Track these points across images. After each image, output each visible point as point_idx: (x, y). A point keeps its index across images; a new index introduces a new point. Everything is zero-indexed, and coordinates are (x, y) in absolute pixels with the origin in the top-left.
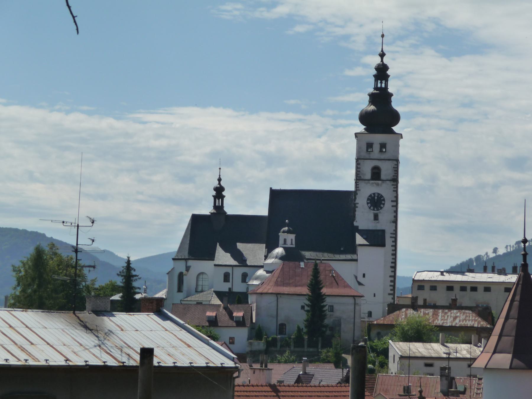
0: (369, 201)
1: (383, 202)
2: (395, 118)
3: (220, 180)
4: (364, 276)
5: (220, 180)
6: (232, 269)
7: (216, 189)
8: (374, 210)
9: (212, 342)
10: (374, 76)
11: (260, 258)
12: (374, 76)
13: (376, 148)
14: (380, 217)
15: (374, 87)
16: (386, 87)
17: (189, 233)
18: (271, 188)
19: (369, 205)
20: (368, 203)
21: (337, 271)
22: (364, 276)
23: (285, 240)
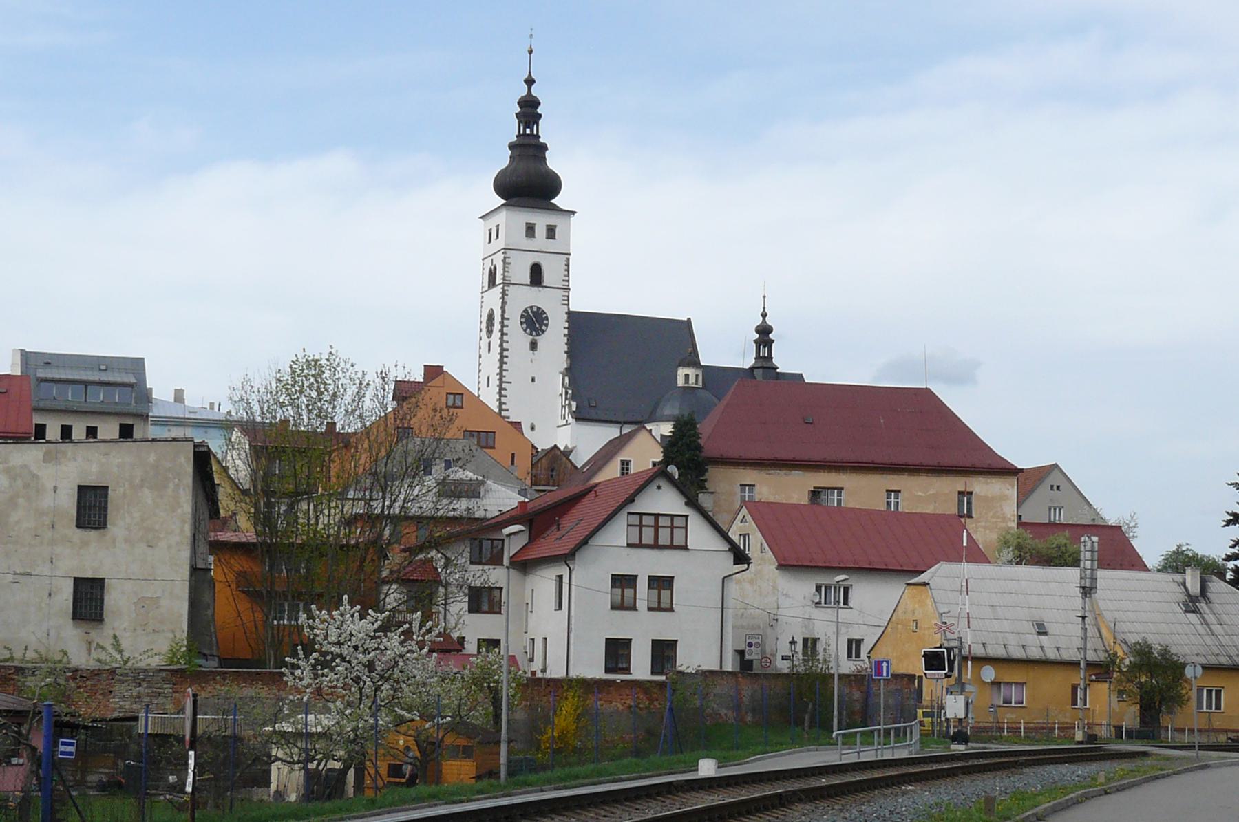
0: (523, 320)
1: (545, 322)
2: (772, 358)
3: (764, 315)
4: (533, 428)
5: (764, 315)
6: (678, 529)
7: (762, 315)
8: (531, 334)
9: (748, 759)
10: (756, 341)
11: (240, 698)
12: (756, 341)
13: (541, 231)
14: (539, 345)
15: (517, 133)
16: (770, 358)
17: (1007, 467)
18: (555, 226)
19: (524, 326)
20: (522, 323)
21: (186, 554)
22: (533, 428)
23: (687, 376)
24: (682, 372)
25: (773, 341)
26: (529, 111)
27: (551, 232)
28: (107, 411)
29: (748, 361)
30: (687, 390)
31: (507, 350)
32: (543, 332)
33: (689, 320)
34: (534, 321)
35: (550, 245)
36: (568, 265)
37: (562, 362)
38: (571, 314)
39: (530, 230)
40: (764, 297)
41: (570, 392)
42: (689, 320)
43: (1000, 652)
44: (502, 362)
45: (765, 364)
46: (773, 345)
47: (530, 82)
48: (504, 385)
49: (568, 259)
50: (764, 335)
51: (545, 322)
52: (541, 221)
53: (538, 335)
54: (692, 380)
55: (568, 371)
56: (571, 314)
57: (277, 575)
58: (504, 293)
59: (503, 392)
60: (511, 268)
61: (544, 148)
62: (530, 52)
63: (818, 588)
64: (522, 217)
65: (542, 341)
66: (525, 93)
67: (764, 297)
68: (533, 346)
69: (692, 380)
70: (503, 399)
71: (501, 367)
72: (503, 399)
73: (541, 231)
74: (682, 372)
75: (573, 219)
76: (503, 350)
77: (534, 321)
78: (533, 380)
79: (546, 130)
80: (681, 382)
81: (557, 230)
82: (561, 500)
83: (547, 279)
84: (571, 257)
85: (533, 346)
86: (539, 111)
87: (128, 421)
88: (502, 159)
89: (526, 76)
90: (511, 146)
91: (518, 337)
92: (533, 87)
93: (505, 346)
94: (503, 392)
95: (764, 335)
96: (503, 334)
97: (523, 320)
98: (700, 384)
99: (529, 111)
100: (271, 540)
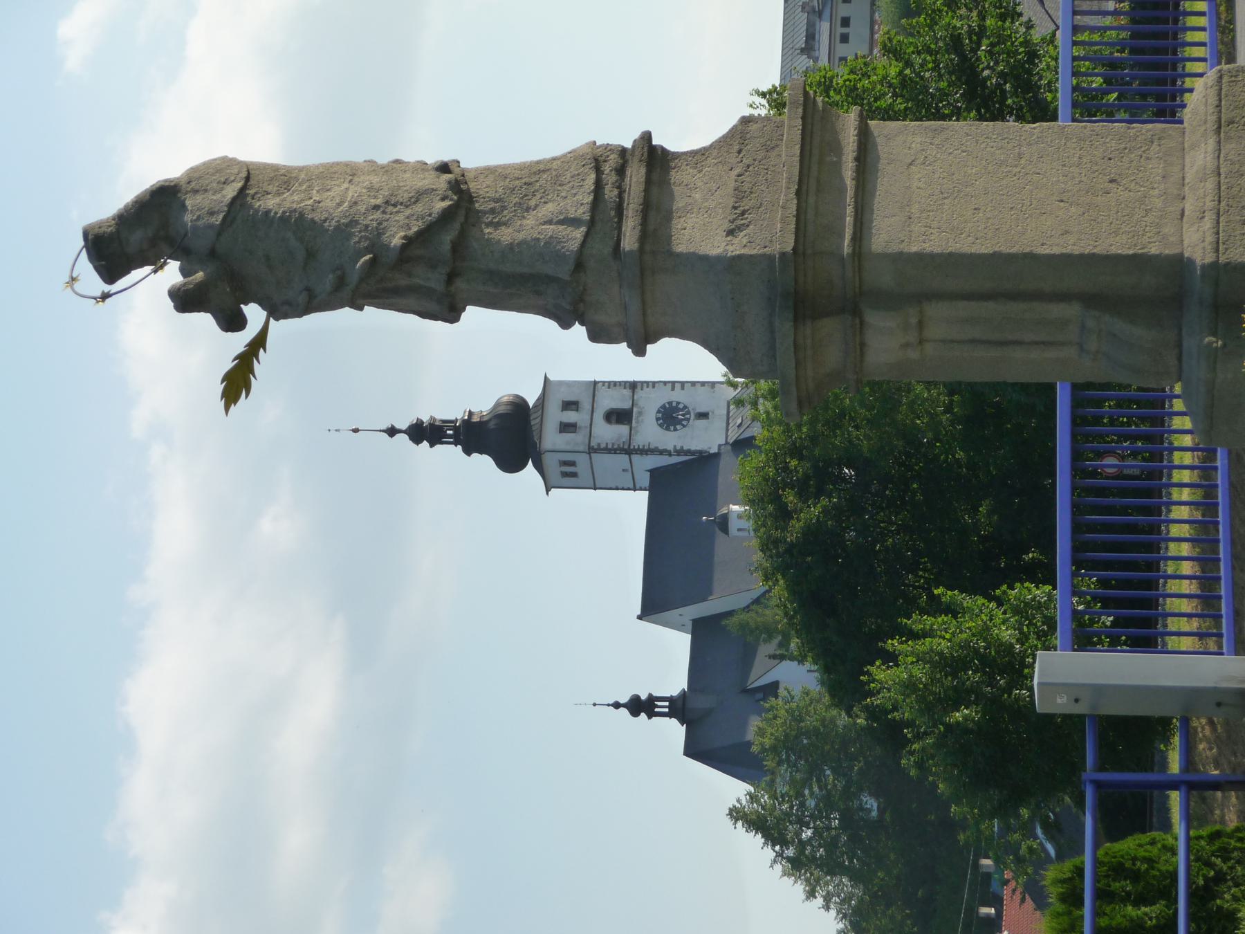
0: (672, 428)
3: (617, 705)
5: (617, 705)
10: (650, 717)
12: (650, 717)
14: (702, 409)
25: (650, 695)
27: (569, 405)
28: (828, 33)
32: (685, 407)
35: (586, 405)
40: (595, 705)
45: (678, 708)
46: (654, 695)
47: (392, 432)
51: (674, 404)
61: (468, 451)
62: (356, 431)
66: (405, 437)
67: (595, 705)
75: (551, 377)
79: (451, 410)
82: (873, 195)
86: (425, 444)
88: (484, 463)
97: (672, 428)
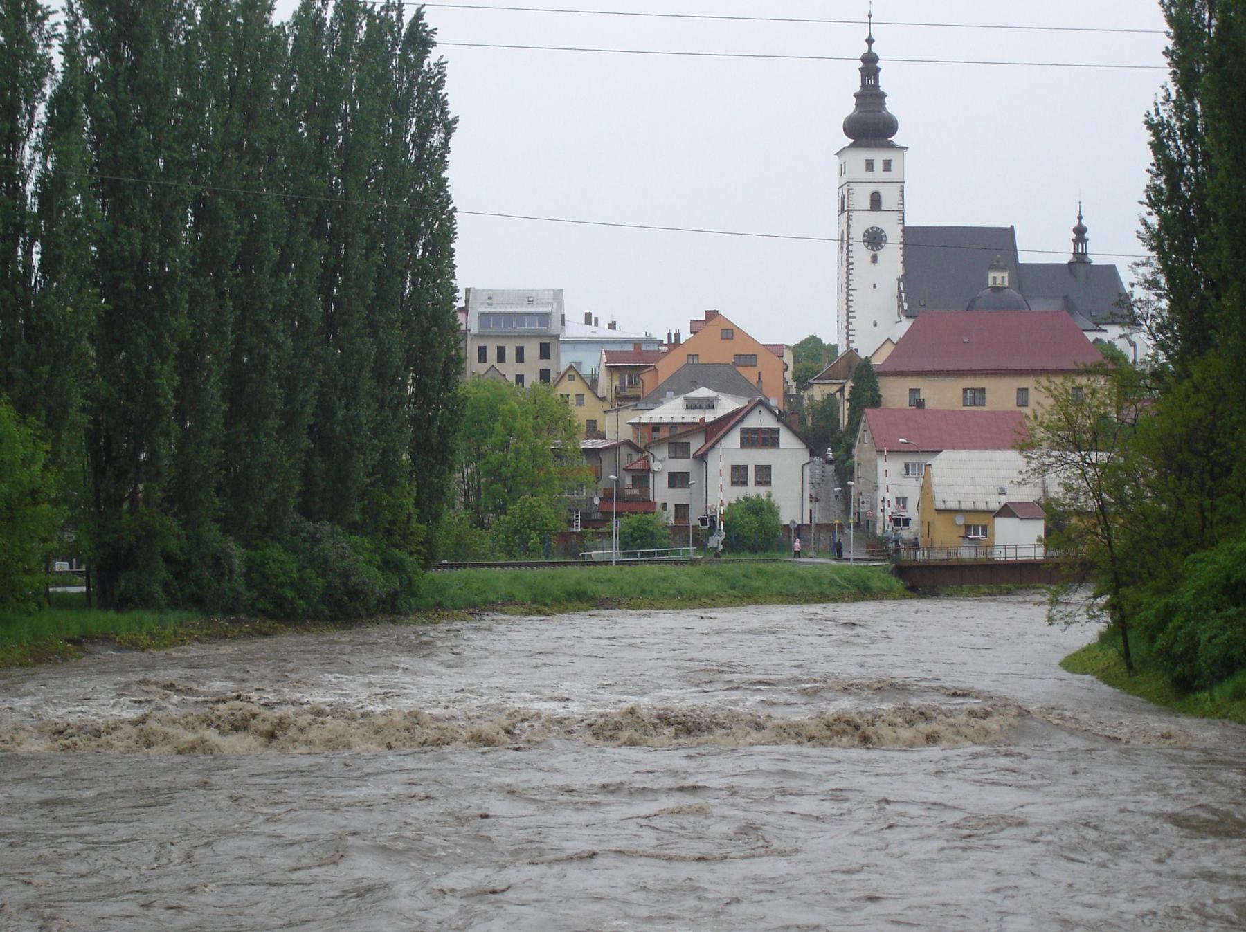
3: (1080, 218)
5: (1080, 218)
13: (878, 166)
14: (879, 258)
23: (994, 278)
24: (991, 275)
26: (870, 65)
27: (887, 166)
29: (1066, 259)
30: (996, 289)
31: (852, 264)
33: (1012, 227)
34: (875, 239)
35: (886, 176)
36: (902, 191)
37: (899, 271)
38: (906, 231)
39: (869, 165)
41: (903, 295)
42: (1012, 227)
43: (969, 506)
44: (848, 274)
45: (1080, 258)
47: (870, 41)
48: (850, 292)
49: (903, 187)
50: (1080, 233)
52: (878, 156)
53: (878, 250)
54: (999, 281)
55: (904, 279)
56: (906, 231)
57: (92, 509)
58: (849, 218)
59: (850, 298)
60: (853, 198)
61: (883, 96)
63: (907, 466)
64: (864, 155)
65: (881, 254)
66: (866, 51)
68: (874, 259)
69: (999, 281)
70: (850, 303)
71: (847, 278)
72: (850, 303)
73: (878, 166)
74: (991, 275)
75: (907, 153)
76: (849, 264)
77: (875, 239)
78: (875, 286)
80: (991, 283)
81: (893, 164)
83: (885, 205)
84: (905, 185)
85: (874, 259)
87: (546, 341)
88: (849, 107)
89: (867, 36)
90: (855, 95)
91: (861, 253)
92: (873, 45)
93: (851, 260)
94: (850, 298)
95: (1080, 233)
96: (848, 251)
98: (1006, 284)
99: (870, 65)
100: (278, 482)
